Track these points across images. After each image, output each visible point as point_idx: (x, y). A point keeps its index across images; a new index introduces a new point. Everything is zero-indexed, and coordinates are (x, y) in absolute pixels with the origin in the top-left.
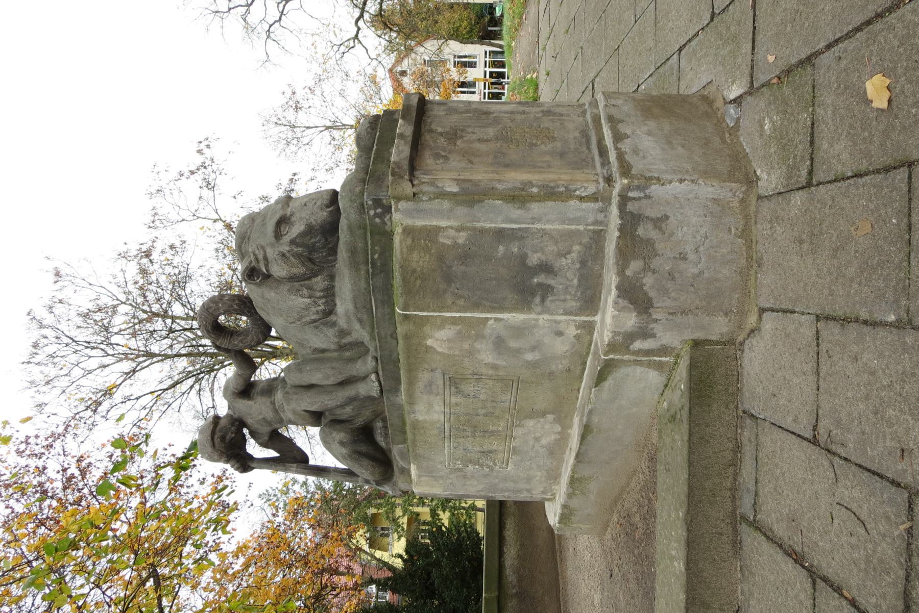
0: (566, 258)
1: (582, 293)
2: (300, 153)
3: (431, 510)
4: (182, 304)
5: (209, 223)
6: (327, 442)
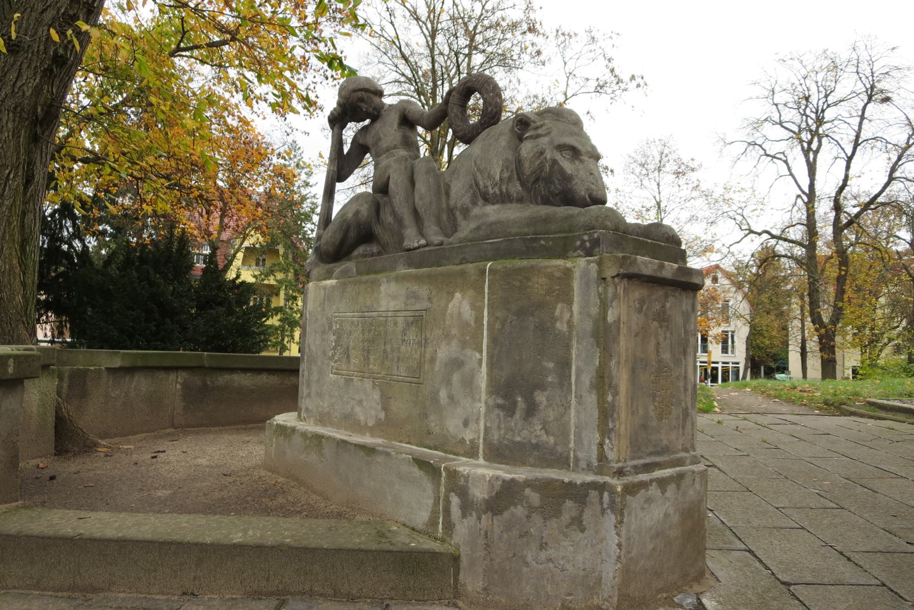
0: (541, 429)
1: (506, 445)
2: (632, 176)
3: (282, 307)
4: (483, 63)
5: (563, 88)
6: (358, 198)
